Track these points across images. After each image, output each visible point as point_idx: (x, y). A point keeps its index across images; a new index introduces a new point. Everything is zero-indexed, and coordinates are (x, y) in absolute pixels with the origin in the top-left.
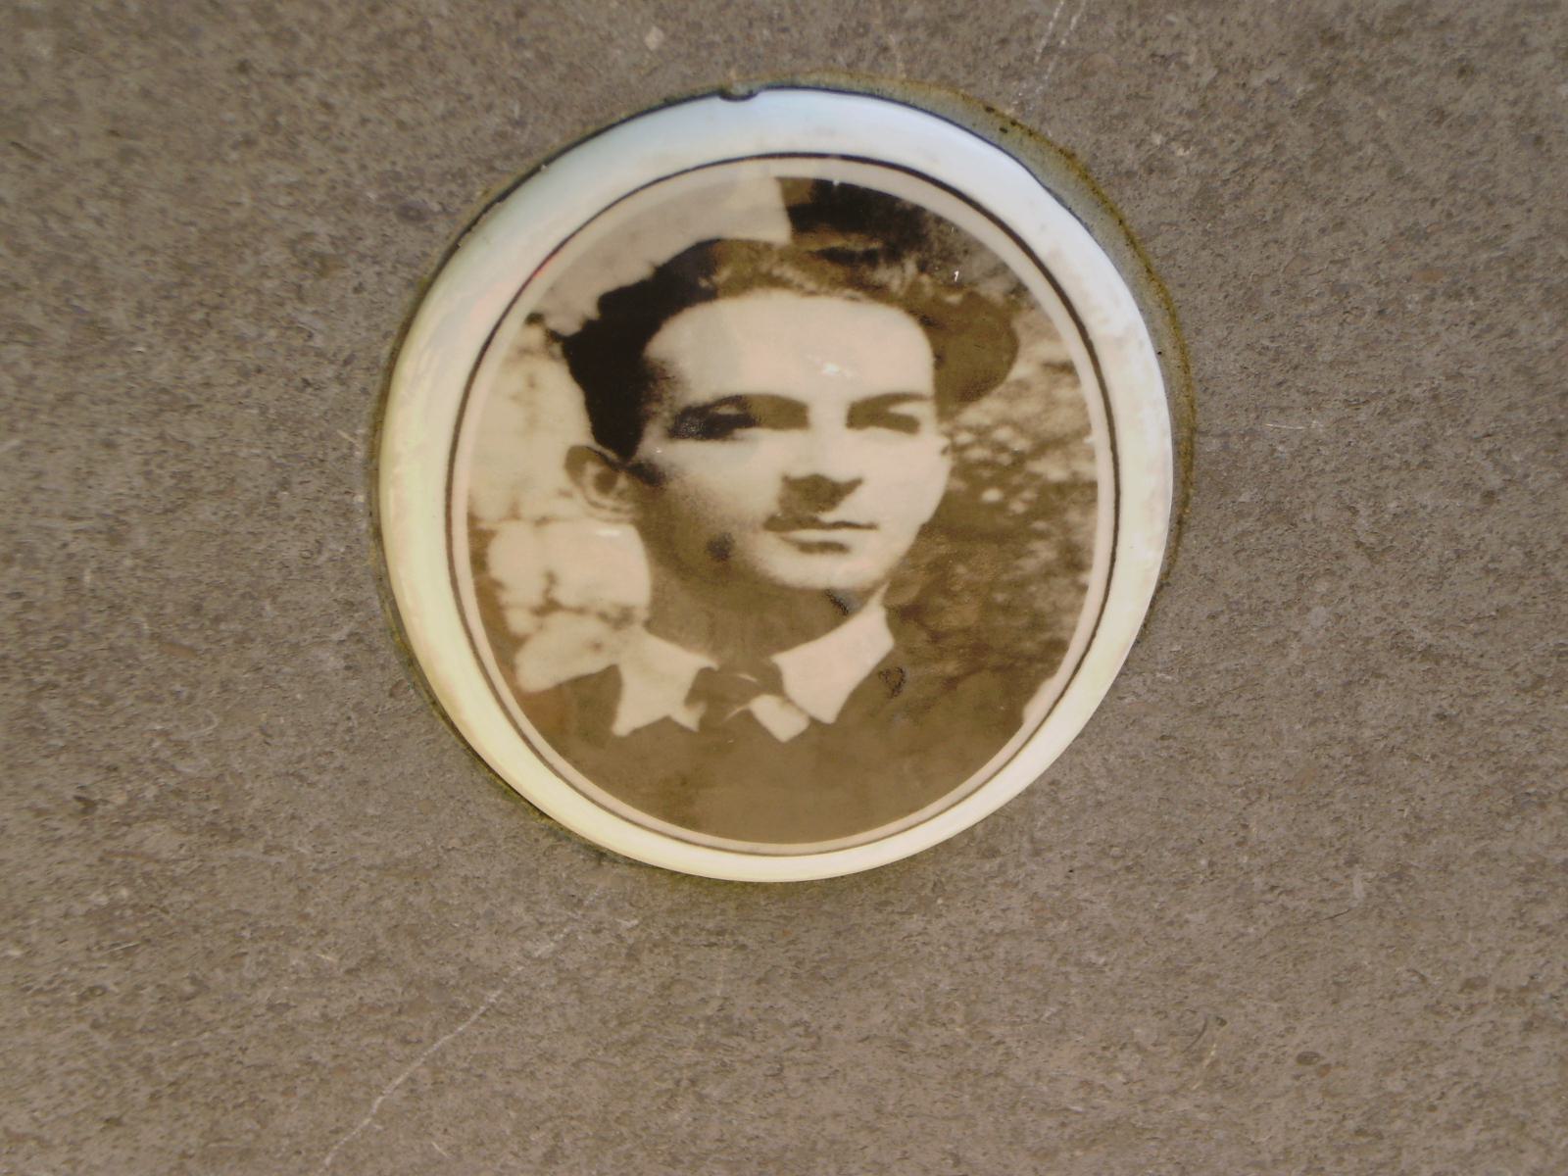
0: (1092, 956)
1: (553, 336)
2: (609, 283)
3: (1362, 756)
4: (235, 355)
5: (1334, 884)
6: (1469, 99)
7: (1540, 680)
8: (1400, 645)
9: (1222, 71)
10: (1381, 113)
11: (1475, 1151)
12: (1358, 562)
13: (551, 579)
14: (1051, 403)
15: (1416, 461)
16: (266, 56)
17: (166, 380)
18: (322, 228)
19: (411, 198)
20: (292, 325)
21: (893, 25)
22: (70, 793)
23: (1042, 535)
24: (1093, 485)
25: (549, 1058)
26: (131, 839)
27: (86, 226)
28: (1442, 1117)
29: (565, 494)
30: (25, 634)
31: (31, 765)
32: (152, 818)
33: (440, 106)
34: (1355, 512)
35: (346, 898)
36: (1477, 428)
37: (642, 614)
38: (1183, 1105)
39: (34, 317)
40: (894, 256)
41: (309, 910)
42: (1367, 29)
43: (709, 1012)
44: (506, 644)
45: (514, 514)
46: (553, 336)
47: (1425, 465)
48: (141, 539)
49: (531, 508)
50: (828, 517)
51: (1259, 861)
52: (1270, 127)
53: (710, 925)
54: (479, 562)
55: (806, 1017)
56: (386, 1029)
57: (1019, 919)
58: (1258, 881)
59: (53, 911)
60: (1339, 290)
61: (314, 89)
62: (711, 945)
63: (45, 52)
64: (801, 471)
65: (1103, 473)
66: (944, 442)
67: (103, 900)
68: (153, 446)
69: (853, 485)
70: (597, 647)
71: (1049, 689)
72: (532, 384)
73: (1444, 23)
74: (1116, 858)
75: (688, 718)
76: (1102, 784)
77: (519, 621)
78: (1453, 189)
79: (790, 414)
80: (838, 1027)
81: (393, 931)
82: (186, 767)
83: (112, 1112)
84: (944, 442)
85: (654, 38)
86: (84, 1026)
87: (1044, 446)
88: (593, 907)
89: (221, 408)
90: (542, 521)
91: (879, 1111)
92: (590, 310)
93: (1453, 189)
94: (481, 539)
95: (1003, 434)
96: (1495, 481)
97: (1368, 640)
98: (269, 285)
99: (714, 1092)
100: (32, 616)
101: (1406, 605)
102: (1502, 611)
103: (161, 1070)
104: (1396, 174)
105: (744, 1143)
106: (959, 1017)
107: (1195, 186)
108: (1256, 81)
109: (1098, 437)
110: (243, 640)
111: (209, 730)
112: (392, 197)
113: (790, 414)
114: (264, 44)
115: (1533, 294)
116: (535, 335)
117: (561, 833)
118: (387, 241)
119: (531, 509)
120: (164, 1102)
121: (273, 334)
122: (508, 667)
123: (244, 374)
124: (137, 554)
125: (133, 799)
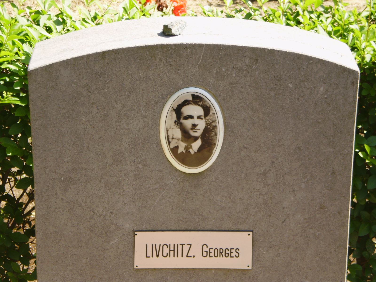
0: (220, 184)
1: (174, 109)
2: (178, 104)
3: (242, 160)
4: (150, 112)
5: (241, 176)
6: (243, 90)
7: (255, 151)
8: (244, 147)
9: (224, 87)
10: (236, 91)
11: (257, 212)
12: (239, 137)
13: (173, 135)
14: (213, 117)
15: (243, 126)
16: (154, 84)
17: (144, 115)
18: (157, 100)
19: (164, 97)
20: (154, 109)
21: (200, 81)
22: (133, 160)
23: (213, 131)
24: (217, 126)
25: (172, 196)
26: (138, 166)
27: (139, 99)
28: (253, 207)
29: (174, 126)
30: (131, 141)
31: (131, 157)
32: (140, 163)
33: (166, 88)
34: (238, 131)
35: (155, 174)
36: (247, 123)
37: (180, 139)
38: (230, 205)
39: (135, 108)
40: (200, 102)
41: (152, 175)
42: (234, 83)
43: (186, 191)
44: (169, 143)
45: (170, 128)
46: (174, 109)
47: (244, 127)
48: (141, 132)
49: (172, 127)
50: (196, 128)
51: (234, 173)
52: (228, 92)
53: (186, 179)
54: (167, 134)
55: (195, 192)
56: (158, 191)
57: (214, 180)
58: (234, 175)
59: (131, 174)
60: (235, 108)
61: (157, 87)
62: (187, 182)
63: (138, 83)
64: (193, 123)
65: (218, 125)
66: (205, 121)
67: (135, 173)
68: (143, 121)
69: (197, 125)
70: (177, 143)
71: (215, 149)
72: (172, 114)
73: (240, 83)
74: (222, 172)
75: (184, 151)
76: (220, 163)
77: (170, 140)
78: (242, 99)
79: (191, 117)
80: (198, 193)
81: (159, 178)
82: (143, 157)
83: (134, 200)
84: (205, 121)
85: (182, 82)
86: (132, 189)
87: (213, 122)
88: (176, 177)
89: (148, 118)
90: (173, 129)
91: (202, 204)
92: (177, 107)
93: (242, 99)
94: (168, 131)
95: (209, 120)
96: (249, 129)
97: (241, 146)
98: (152, 105)
99: (187, 201)
100: (132, 140)
101: (243, 142)
102: (251, 143)
103: (138, 195)
104: (238, 97)
105: (190, 208)
106: (209, 192)
107: (223, 97)
108: (227, 87)
109: (217, 121)
110: (148, 143)
111: (145, 153)
112: (162, 97)
113: (191, 117)
114: (154, 83)
115: (250, 109)
116: (172, 109)
117: (177, 170)
118: (161, 101)
119: (172, 128)
120: (138, 199)
121: (152, 110)
122: (169, 144)
123: (150, 114)
124: (141, 133)
125: (138, 161)
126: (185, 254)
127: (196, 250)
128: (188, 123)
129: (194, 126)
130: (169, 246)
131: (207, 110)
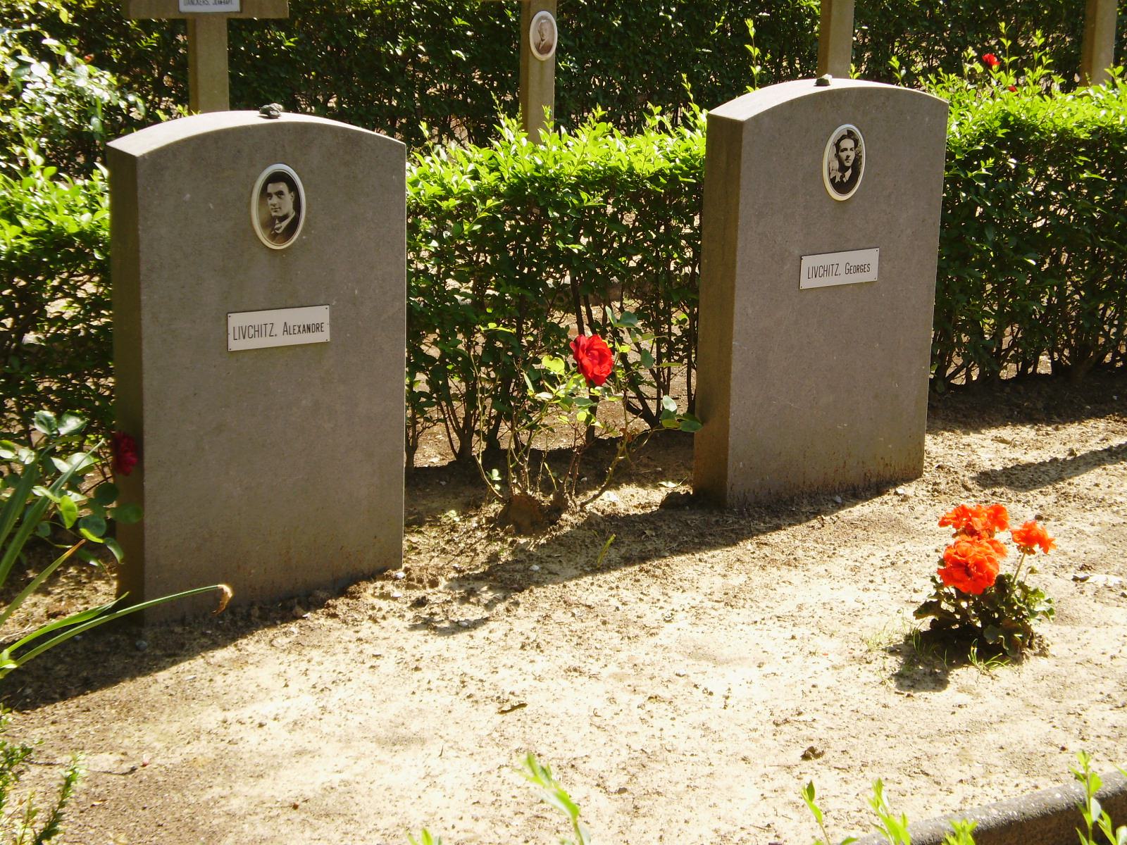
79: (846, 149)
113: (846, 149)
126: (268, 333)
127: (278, 329)
128: (843, 155)
129: (848, 157)
130: (253, 327)
131: (856, 142)
